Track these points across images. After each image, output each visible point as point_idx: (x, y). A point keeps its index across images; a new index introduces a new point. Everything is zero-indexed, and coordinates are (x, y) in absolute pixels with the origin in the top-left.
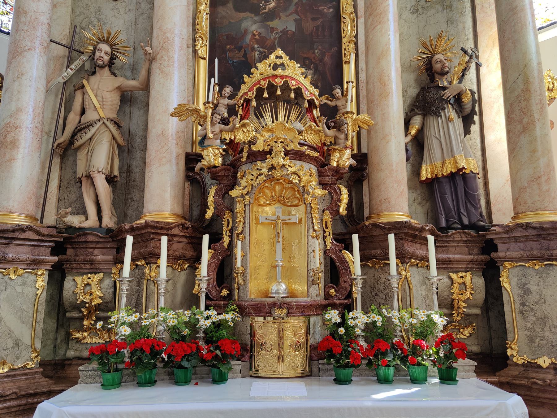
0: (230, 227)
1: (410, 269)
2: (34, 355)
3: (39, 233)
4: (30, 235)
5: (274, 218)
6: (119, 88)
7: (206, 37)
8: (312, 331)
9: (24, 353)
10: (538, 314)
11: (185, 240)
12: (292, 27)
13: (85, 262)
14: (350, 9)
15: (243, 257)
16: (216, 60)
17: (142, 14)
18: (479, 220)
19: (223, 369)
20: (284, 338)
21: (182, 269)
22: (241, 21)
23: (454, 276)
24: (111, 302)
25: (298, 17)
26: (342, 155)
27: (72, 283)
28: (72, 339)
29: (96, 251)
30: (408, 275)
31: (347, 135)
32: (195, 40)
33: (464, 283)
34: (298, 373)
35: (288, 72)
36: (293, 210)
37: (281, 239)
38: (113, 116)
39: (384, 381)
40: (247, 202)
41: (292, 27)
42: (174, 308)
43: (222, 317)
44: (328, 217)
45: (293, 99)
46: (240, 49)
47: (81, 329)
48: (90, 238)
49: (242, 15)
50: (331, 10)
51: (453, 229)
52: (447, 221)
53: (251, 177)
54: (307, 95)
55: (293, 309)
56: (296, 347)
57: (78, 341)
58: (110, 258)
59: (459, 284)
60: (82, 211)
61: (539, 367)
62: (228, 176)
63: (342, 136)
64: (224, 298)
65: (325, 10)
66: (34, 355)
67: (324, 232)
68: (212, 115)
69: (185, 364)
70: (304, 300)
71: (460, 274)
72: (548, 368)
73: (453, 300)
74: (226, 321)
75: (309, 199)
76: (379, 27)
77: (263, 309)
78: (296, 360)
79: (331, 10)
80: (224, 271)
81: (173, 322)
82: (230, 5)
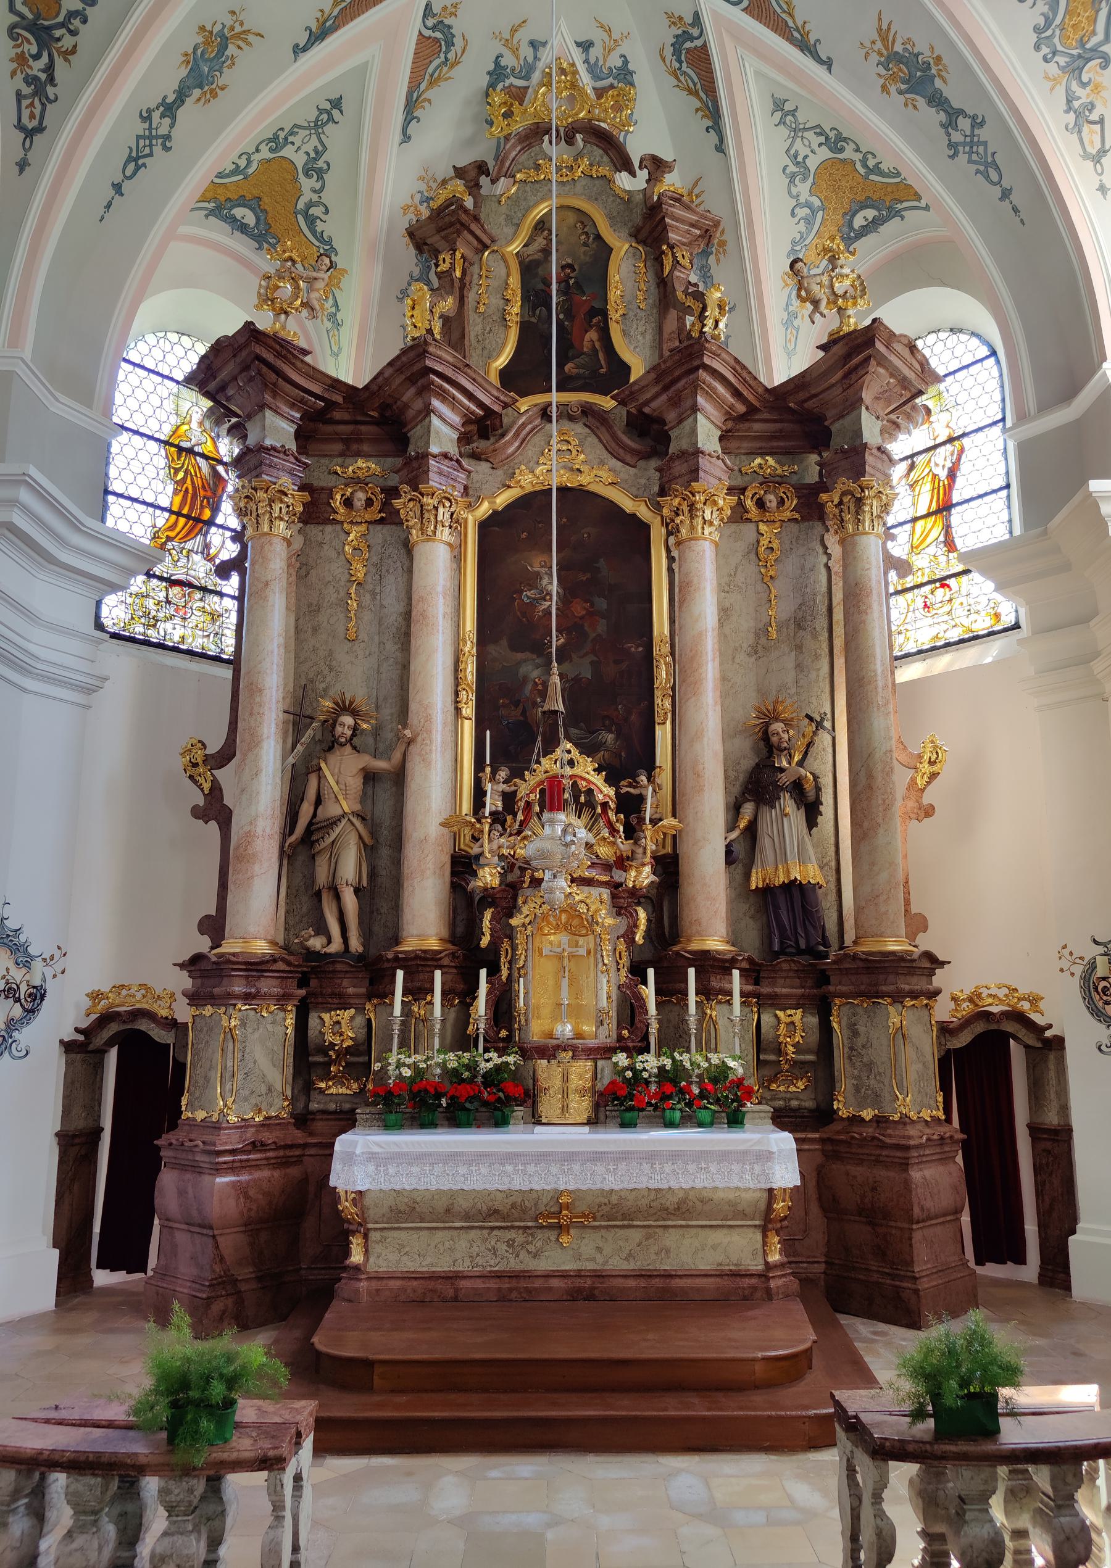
0: (509, 957)
1: (718, 1007)
2: (286, 1103)
3: (289, 963)
4: (281, 966)
5: (559, 950)
6: (363, 769)
7: (471, 688)
8: (599, 1076)
9: (276, 1101)
10: (865, 1060)
11: (454, 971)
12: (587, 674)
13: (333, 995)
14: (666, 649)
15: (525, 994)
16: (488, 732)
17: (387, 659)
18: (819, 944)
19: (506, 1111)
20: (568, 1082)
21: (452, 1006)
22: (519, 664)
23: (780, 1013)
24: (363, 1044)
25: (595, 659)
26: (639, 873)
27: (318, 1021)
28: (315, 1089)
29: (345, 983)
30: (714, 1013)
31: (645, 848)
32: (457, 694)
33: (793, 1023)
34: (583, 1118)
35: (578, 770)
36: (581, 941)
37: (566, 974)
38: (357, 807)
39: (670, 1125)
40: (529, 932)
41: (587, 674)
42: (452, 1049)
43: (504, 1059)
44: (622, 946)
45: (584, 802)
46: (517, 704)
47: (327, 1076)
48: (339, 967)
49: (520, 656)
50: (640, 649)
51: (786, 954)
52: (781, 943)
53: (534, 905)
54: (600, 797)
55: (579, 1051)
56: (582, 1092)
57: (321, 1091)
58: (363, 990)
59: (787, 1024)
60: (322, 929)
61: (863, 1120)
62: (507, 898)
63: (640, 850)
64: (503, 1040)
65: (633, 649)
66: (286, 1103)
67: (618, 964)
68: (490, 832)
69: (468, 1105)
70: (592, 1043)
71: (789, 1012)
72: (870, 1121)
73: (780, 1043)
74: (507, 1063)
75: (598, 930)
76: (693, 699)
77: (548, 1052)
78: (581, 1107)
79: (640, 649)
80: (503, 1008)
81: (452, 1065)
82: (504, 642)
